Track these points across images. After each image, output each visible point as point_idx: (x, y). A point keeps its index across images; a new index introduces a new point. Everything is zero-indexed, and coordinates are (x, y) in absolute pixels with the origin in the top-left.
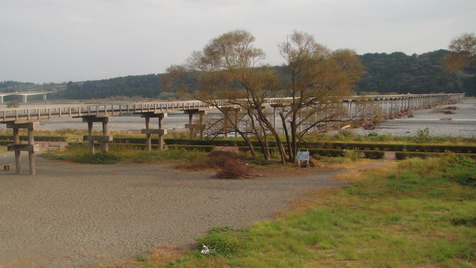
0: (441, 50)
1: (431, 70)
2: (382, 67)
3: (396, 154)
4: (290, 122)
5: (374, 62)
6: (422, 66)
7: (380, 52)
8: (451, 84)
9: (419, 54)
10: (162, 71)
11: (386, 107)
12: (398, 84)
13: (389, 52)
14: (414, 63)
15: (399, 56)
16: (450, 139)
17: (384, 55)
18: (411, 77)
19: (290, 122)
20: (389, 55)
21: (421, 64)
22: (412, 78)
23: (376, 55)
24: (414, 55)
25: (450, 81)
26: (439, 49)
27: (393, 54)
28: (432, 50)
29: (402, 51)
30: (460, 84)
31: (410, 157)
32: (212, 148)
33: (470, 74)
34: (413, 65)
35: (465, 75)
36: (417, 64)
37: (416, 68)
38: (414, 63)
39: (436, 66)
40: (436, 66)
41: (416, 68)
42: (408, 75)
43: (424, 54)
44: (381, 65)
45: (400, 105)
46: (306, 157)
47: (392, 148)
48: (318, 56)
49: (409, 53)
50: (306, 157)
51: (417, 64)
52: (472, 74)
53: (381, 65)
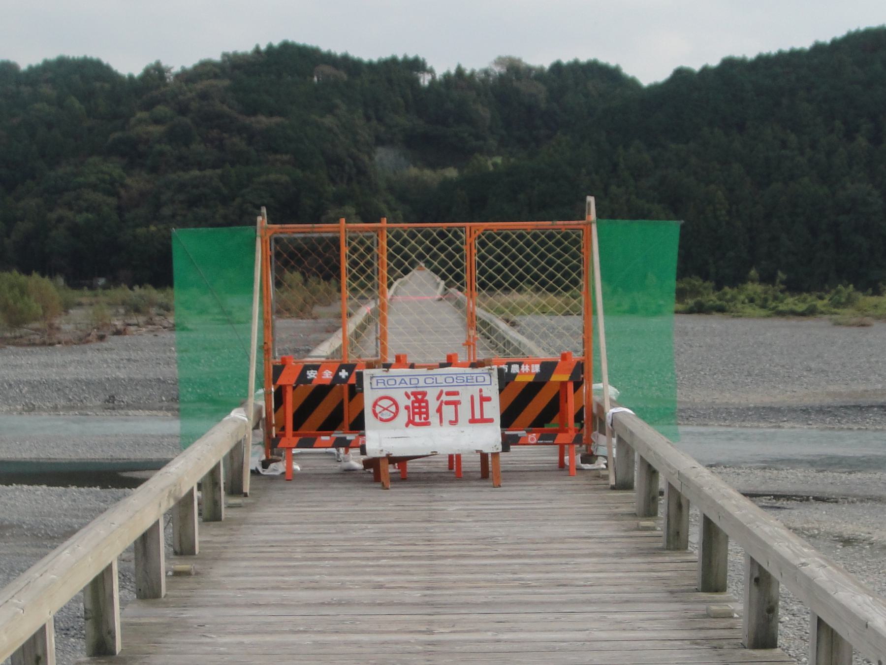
1: (238, 142)
4: (260, 444)
6: (187, 120)
9: (177, 69)
12: (53, 216)
14: (149, 106)
15: (81, 80)
18: (128, 181)
19: (260, 444)
21: (183, 110)
22: (137, 182)
24: (155, 75)
26: (276, 43)
27: (47, 66)
28: (245, 47)
29: (93, 53)
31: (454, 460)
33: (433, 166)
34: (141, 115)
35: (413, 171)
36: (161, 110)
37: (156, 130)
38: (149, 106)
39: (263, 121)
40: (263, 121)
41: (156, 130)
42: (113, 168)
48: (743, 562)
49: (129, 64)
51: (161, 110)
52: (444, 166)
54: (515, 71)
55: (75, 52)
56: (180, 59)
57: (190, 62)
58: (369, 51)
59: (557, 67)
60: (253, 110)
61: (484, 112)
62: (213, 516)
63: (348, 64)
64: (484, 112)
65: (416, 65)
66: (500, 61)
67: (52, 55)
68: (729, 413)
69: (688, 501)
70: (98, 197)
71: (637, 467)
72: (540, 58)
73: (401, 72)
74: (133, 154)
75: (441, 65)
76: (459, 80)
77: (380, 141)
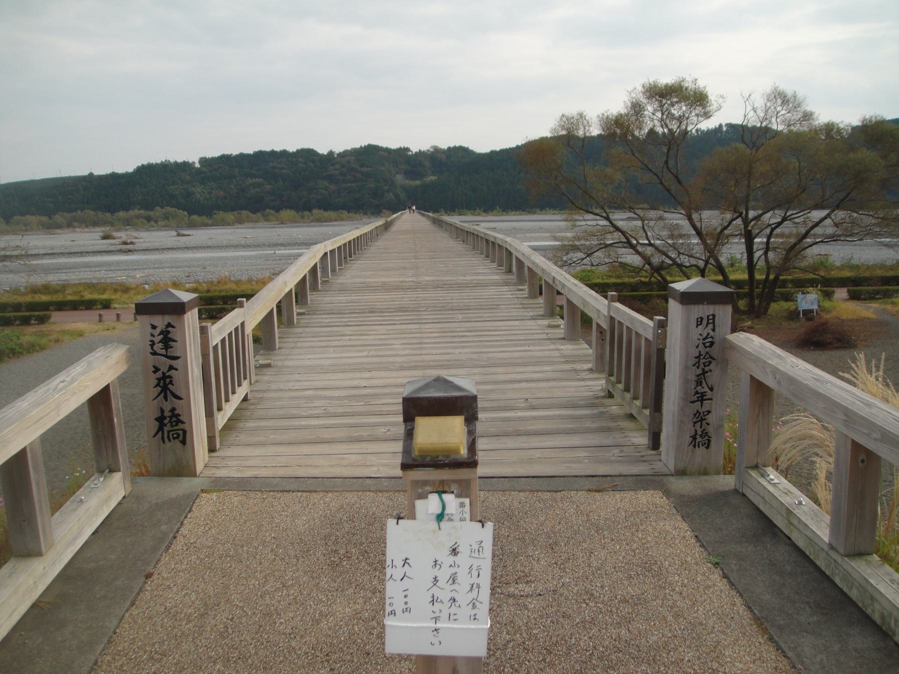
0: (370, 146)
1: (359, 176)
2: (284, 171)
3: (848, 291)
5: (271, 165)
7: (278, 149)
8: (391, 196)
9: (337, 152)
10: (131, 169)
11: (621, 223)
13: (292, 149)
14: (333, 165)
15: (307, 154)
16: (882, 266)
17: (284, 153)
20: (889, 121)
21: (343, 166)
22: (333, 187)
23: (273, 153)
24: (331, 153)
25: (388, 191)
29: (311, 147)
30: (403, 196)
32: (833, 292)
33: (413, 180)
34: (332, 168)
36: (337, 166)
39: (365, 169)
40: (365, 169)
41: (337, 172)
42: (326, 183)
43: (346, 152)
44: (282, 168)
45: (464, 225)
46: (812, 304)
47: (842, 282)
49: (323, 150)
50: (812, 304)
51: (337, 166)
53: (282, 168)
54: (437, 150)
55: (306, 146)
56: (338, 149)
57: (341, 150)
58: (394, 146)
59: (449, 148)
60: (362, 166)
61: (427, 163)
62: (314, 287)
63: (388, 150)
64: (427, 163)
65: (407, 149)
66: (432, 147)
67: (299, 148)
68: (702, 398)
69: (663, 94)
70: (323, 191)
71: (514, 262)
72: (444, 146)
73: (403, 152)
74: (331, 179)
75: (414, 149)
76: (421, 154)
77: (398, 173)
